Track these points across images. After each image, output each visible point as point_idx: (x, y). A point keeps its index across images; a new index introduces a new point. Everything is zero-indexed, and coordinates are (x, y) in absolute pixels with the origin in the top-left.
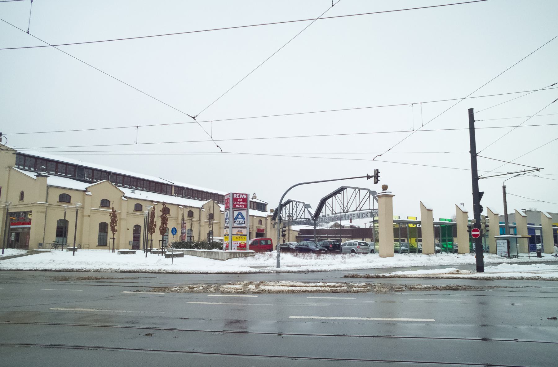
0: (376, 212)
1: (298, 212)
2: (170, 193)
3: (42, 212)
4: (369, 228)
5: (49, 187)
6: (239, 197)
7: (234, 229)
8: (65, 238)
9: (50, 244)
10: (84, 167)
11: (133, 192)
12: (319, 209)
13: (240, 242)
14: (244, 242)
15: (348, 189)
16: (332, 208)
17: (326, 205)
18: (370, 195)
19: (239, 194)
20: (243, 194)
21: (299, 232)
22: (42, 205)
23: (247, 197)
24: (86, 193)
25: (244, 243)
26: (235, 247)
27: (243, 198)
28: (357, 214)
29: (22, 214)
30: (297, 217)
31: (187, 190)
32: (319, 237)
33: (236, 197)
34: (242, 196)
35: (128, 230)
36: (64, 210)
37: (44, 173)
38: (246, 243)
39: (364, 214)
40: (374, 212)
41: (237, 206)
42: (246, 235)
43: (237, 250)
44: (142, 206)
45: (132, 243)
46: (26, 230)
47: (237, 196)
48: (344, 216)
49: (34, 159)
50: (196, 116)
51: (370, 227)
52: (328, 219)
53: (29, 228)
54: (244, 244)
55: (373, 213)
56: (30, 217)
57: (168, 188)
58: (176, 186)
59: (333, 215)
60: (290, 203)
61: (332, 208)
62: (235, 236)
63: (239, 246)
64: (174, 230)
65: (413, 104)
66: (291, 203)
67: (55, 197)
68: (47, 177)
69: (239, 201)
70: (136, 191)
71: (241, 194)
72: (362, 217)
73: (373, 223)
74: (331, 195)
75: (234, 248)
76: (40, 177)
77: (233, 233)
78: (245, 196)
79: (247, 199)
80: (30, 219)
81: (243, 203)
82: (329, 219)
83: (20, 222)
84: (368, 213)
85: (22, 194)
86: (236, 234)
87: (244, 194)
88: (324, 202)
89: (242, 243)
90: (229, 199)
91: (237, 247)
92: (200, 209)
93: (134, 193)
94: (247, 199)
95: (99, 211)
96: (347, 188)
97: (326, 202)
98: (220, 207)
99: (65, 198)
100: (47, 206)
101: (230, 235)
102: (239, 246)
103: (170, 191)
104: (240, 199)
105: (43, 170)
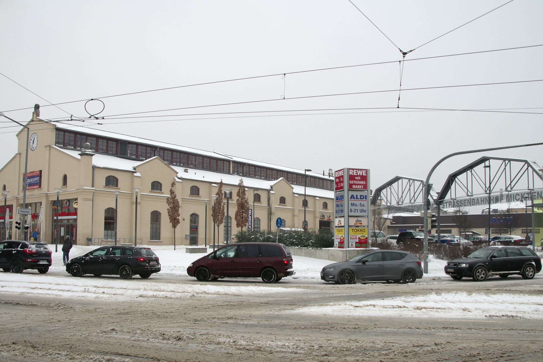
0: (538, 192)
1: (412, 195)
2: (228, 171)
3: (88, 200)
4: (480, 214)
5: (94, 168)
6: (357, 173)
7: (350, 219)
8: (114, 232)
9: (99, 239)
10: (127, 142)
11: (186, 171)
12: (444, 190)
13: (360, 236)
14: (365, 236)
15: (490, 160)
16: (467, 189)
17: (455, 182)
18: (528, 167)
19: (357, 169)
20: (361, 170)
21: (392, 221)
22: (88, 190)
23: (366, 174)
24: (135, 174)
25: (364, 238)
26: (353, 243)
27: (361, 174)
28: (507, 196)
29: (66, 203)
30: (410, 201)
31: (248, 167)
32: (420, 227)
33: (352, 174)
34: (360, 173)
35: (184, 220)
36: (115, 196)
37: (89, 151)
38: (367, 238)
39: (517, 196)
40: (535, 193)
41: (354, 186)
42: (344, 226)
43: (356, 247)
44: (198, 189)
45: (188, 237)
46: (71, 222)
47: (353, 173)
48: (486, 198)
49: (73, 135)
50: (401, 51)
51: (483, 212)
52: (461, 203)
53: (76, 220)
54: (365, 239)
55: (534, 194)
56: (75, 206)
57: (225, 165)
58: (234, 162)
59: (469, 197)
60: (399, 181)
61: (467, 189)
62: (338, 228)
63: (358, 241)
64: (279, 220)
65: (285, 74)
66: (400, 181)
67: (101, 181)
68: (92, 155)
69: (357, 180)
70: (190, 170)
71: (359, 170)
72: (515, 200)
73: (531, 208)
74: (466, 169)
75: (352, 245)
76: (85, 157)
77: (350, 224)
78: (364, 173)
79: (366, 176)
80: (76, 209)
81: (362, 182)
82: (462, 203)
83: (65, 212)
84: (524, 194)
85: (65, 177)
86: (354, 225)
87: (363, 170)
88: (453, 179)
89: (362, 238)
90: (342, 176)
91: (356, 243)
92: (268, 191)
93: (187, 172)
94: (366, 176)
95: (160, 197)
96: (489, 160)
97: (456, 178)
98: (293, 188)
99: (112, 181)
100: (93, 192)
101: (346, 227)
102: (358, 241)
103: (228, 168)
104: (357, 176)
105: (87, 148)
